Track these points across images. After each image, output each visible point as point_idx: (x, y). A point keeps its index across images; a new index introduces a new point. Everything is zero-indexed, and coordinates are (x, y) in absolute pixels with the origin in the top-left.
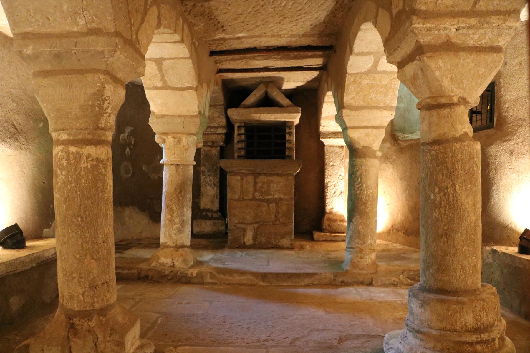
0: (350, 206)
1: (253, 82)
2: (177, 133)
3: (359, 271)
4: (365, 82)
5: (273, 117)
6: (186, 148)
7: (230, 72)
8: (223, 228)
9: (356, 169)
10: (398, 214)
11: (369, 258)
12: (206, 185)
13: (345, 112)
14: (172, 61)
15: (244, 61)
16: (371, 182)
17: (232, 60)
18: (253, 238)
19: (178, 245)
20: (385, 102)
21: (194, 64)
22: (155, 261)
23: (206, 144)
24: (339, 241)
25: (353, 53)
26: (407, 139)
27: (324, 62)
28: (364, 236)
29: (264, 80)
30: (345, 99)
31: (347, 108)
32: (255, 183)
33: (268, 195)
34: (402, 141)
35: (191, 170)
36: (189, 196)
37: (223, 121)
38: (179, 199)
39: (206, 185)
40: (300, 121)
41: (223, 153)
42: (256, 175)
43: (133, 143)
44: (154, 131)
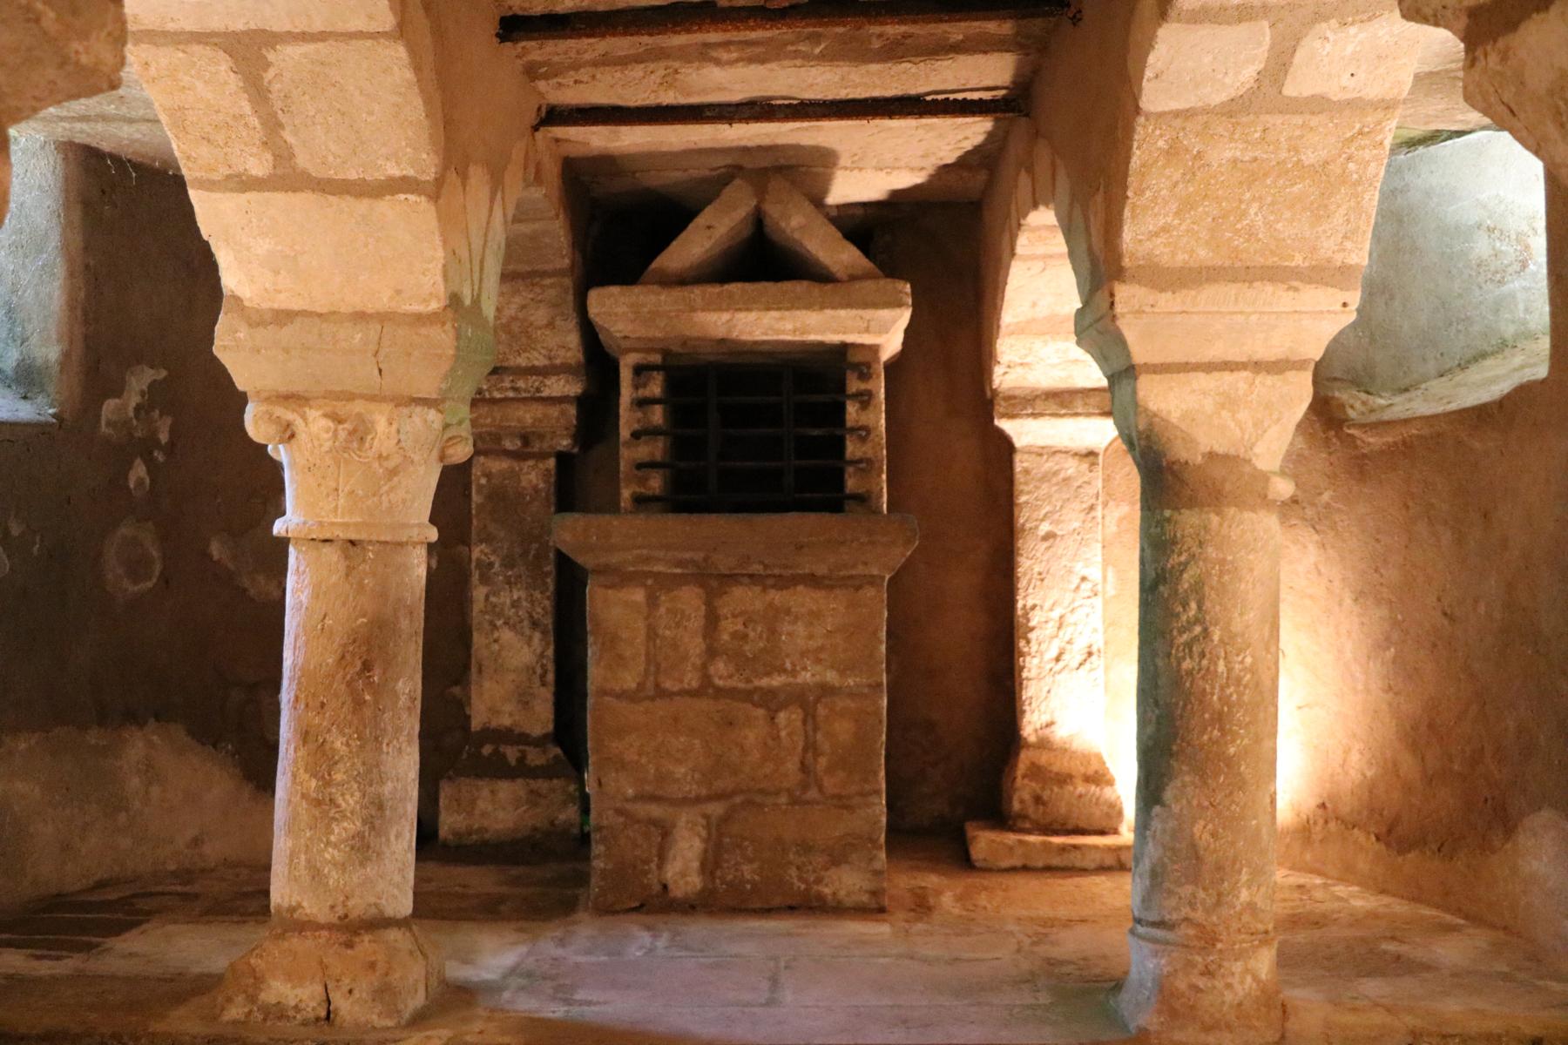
0: (1150, 729)
1: (699, 171)
2: (351, 397)
3: (1202, 1037)
4: (1223, 153)
5: (789, 326)
6: (391, 464)
7: (595, 122)
8: (570, 814)
9: (1175, 560)
10: (1347, 751)
11: (1247, 971)
12: (495, 627)
13: (1127, 295)
14: (310, 48)
15: (660, 69)
16: (1246, 620)
17: (605, 61)
18: (703, 865)
19: (353, 915)
20: (1314, 249)
21: (417, 69)
22: (240, 999)
23: (486, 444)
24: (1083, 871)
25: (1173, 13)
26: (1387, 416)
27: (1018, 74)
28: (1219, 868)
29: (748, 163)
30: (1128, 235)
31: (1137, 279)
32: (712, 621)
33: (768, 674)
34: (1362, 426)
35: (418, 567)
36: (408, 685)
37: (570, 345)
38: (359, 703)
39: (495, 627)
40: (904, 344)
41: (574, 485)
42: (714, 582)
43: (164, 437)
44: (240, 386)
